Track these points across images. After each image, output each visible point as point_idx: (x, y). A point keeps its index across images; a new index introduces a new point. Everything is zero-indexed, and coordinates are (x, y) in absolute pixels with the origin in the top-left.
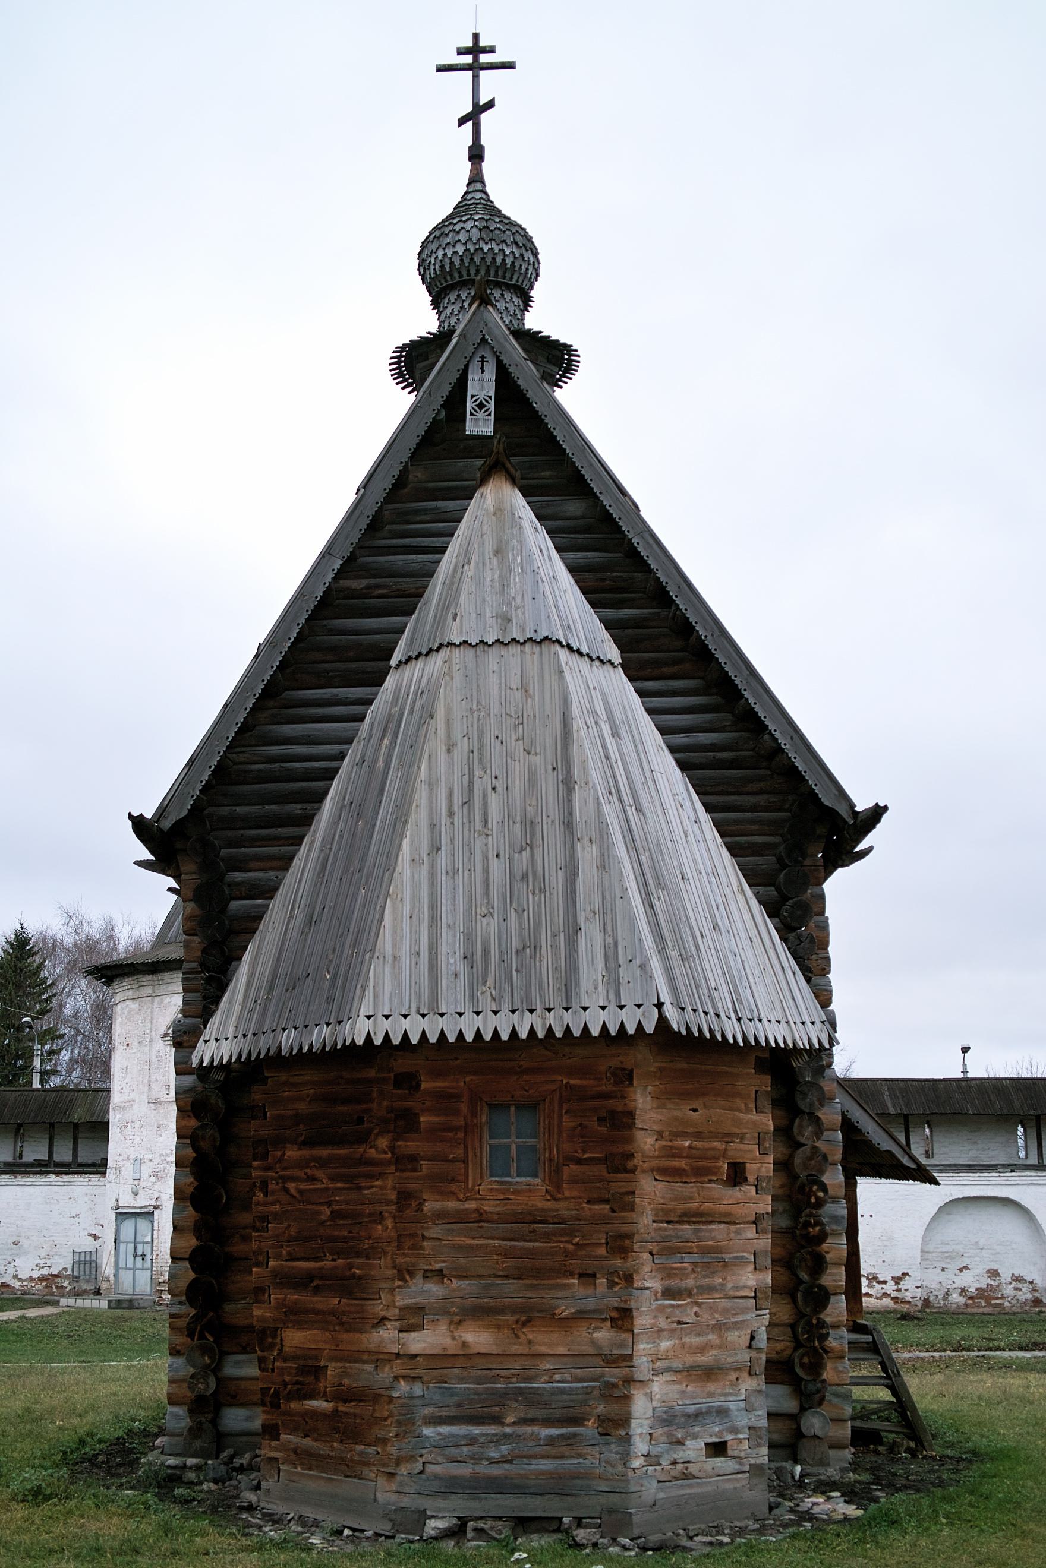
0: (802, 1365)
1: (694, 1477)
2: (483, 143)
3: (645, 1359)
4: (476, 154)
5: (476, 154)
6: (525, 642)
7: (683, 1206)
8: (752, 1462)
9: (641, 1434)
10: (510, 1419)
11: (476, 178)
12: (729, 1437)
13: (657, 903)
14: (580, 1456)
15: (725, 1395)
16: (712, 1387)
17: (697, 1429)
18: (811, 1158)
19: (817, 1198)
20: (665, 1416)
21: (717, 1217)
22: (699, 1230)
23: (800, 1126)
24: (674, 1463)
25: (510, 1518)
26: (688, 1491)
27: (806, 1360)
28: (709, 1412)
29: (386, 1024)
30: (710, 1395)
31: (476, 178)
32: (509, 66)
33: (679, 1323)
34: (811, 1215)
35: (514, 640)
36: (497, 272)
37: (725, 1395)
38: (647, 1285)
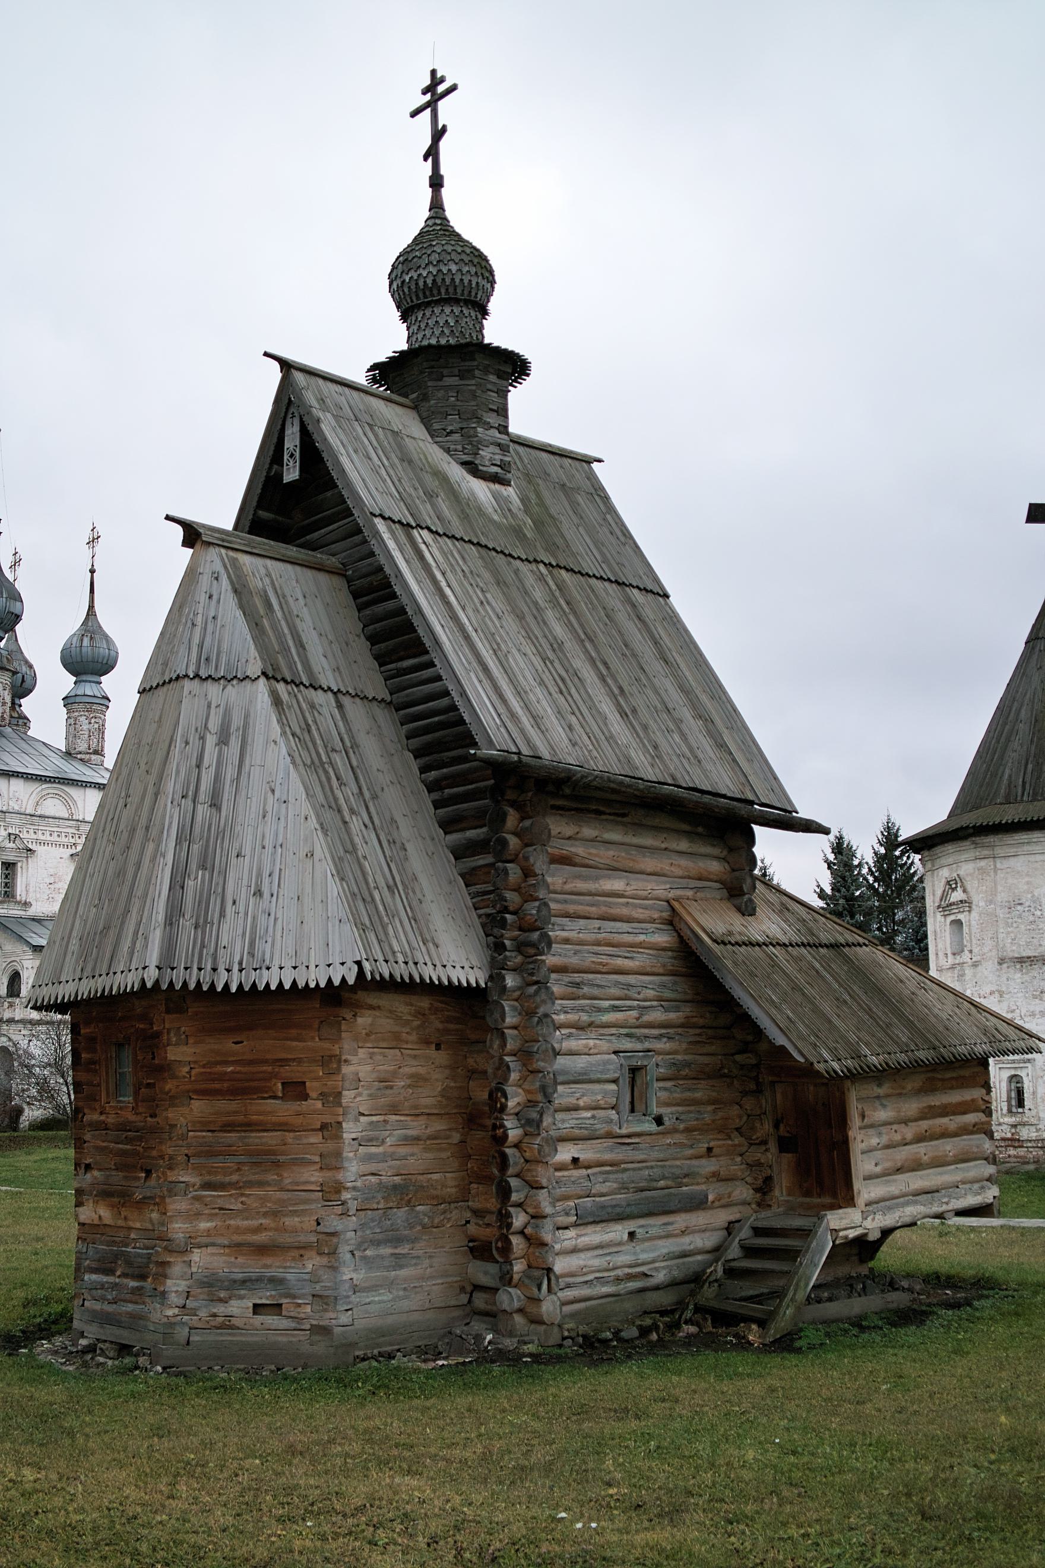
0: (497, 1248)
1: (238, 1328)
2: (442, 172)
3: (182, 1235)
4: (436, 182)
5: (436, 182)
6: (207, 679)
7: (224, 1119)
8: (314, 1322)
9: (177, 1292)
10: (118, 1273)
11: (437, 206)
12: (283, 1301)
13: (191, 883)
14: (144, 1303)
15: (285, 1268)
16: (268, 1261)
17: (243, 1292)
18: (498, 1069)
19: (502, 1104)
20: (205, 1280)
21: (269, 1127)
22: (245, 1137)
23: (491, 1040)
24: (215, 1315)
25: (116, 1343)
26: (230, 1338)
27: (500, 1244)
28: (259, 1280)
29: (253, 975)
30: (266, 1266)
31: (437, 206)
32: (453, 88)
33: (221, 1209)
34: (497, 1118)
35: (210, 676)
36: (424, 293)
37: (285, 1268)
38: (182, 1179)
